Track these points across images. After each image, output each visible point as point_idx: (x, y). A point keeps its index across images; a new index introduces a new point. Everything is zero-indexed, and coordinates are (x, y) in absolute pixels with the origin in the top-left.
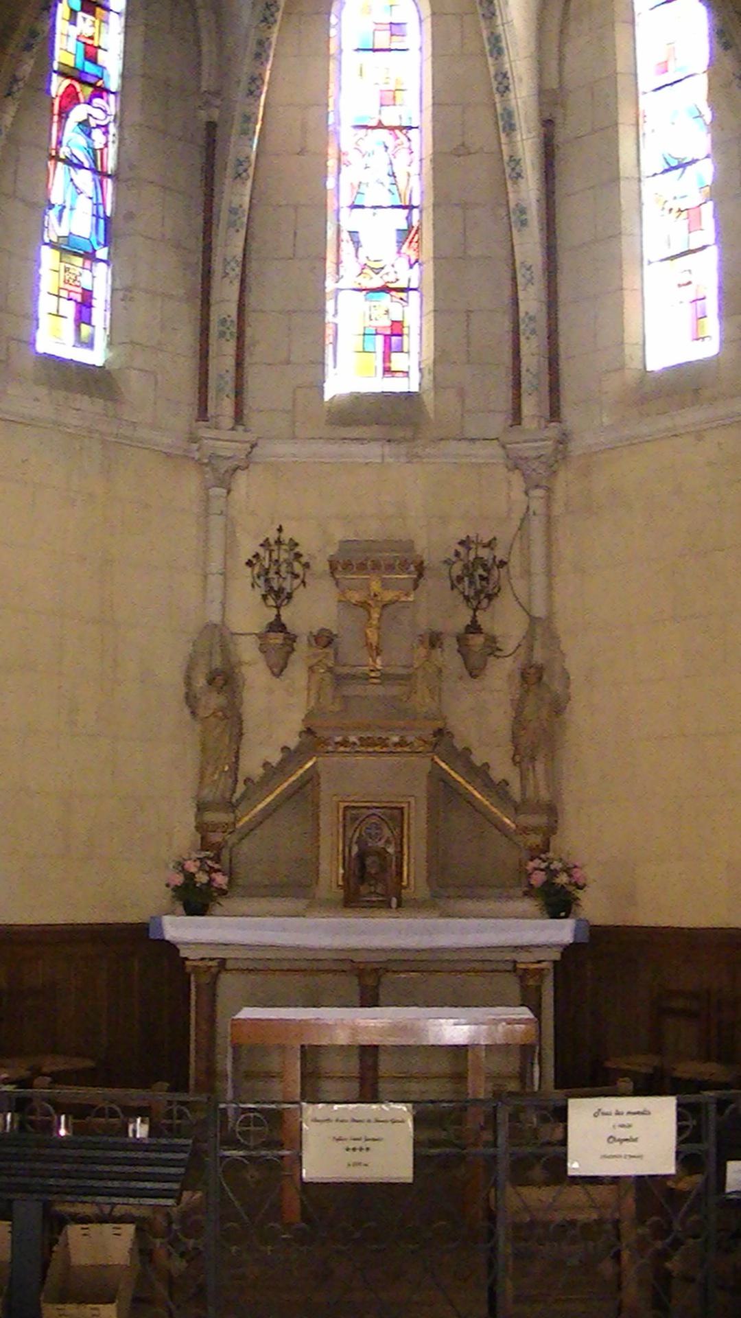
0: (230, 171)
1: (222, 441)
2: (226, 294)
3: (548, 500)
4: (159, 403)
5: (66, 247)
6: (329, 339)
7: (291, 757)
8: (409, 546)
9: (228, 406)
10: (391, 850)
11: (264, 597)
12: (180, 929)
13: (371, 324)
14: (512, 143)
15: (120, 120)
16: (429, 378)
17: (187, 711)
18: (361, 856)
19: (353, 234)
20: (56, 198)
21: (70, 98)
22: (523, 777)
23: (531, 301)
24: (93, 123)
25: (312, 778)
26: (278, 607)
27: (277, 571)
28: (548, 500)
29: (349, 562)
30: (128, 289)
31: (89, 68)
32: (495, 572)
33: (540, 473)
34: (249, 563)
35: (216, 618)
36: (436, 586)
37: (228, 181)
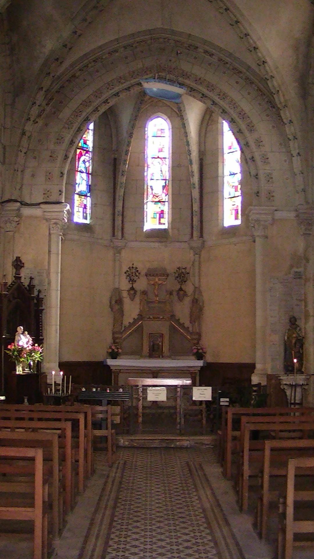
0: (120, 174)
1: (119, 243)
2: (119, 208)
3: (200, 257)
4: (103, 231)
5: (80, 194)
6: (145, 215)
7: (135, 321)
8: (165, 270)
9: (120, 234)
10: (160, 344)
11: (129, 281)
12: (110, 362)
13: (155, 215)
14: (192, 167)
15: (92, 159)
16: (170, 226)
17: (110, 309)
18: (153, 345)
19: (151, 186)
20: (77, 182)
21: (81, 155)
22: (193, 327)
23: (196, 207)
24: (86, 161)
25: (141, 326)
26: (132, 284)
27: (132, 274)
28: (200, 257)
29: (150, 274)
30: (95, 204)
31: (85, 146)
32: (186, 276)
33: (197, 252)
34: (125, 273)
35: (117, 286)
36: (171, 279)
37: (120, 176)
